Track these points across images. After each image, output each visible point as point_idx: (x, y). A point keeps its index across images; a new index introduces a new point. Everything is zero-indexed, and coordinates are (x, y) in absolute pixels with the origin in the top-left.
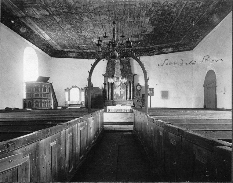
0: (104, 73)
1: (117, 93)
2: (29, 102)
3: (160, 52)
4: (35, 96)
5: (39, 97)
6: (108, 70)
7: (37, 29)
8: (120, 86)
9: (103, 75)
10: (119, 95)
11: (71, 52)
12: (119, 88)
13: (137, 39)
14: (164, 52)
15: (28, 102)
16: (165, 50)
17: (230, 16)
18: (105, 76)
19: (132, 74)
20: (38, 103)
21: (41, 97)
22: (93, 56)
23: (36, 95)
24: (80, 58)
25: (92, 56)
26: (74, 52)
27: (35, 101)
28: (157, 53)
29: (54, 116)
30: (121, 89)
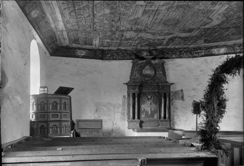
0: (127, 80)
1: (146, 110)
2: (42, 126)
3: (207, 53)
4: (52, 117)
5: (59, 119)
6: (133, 77)
7: (53, 13)
8: (150, 100)
9: (126, 84)
10: (150, 113)
11: (80, 49)
12: (149, 102)
13: (188, 35)
14: (213, 53)
15: (40, 126)
16: (215, 51)
17: (41, 1)
18: (129, 84)
19: (168, 82)
20: (57, 128)
21: (61, 118)
22: (110, 56)
23: (53, 116)
24: (62, 57)
25: (109, 55)
26: (84, 49)
27: (51, 124)
28: (203, 54)
29: (113, 151)
30: (152, 103)
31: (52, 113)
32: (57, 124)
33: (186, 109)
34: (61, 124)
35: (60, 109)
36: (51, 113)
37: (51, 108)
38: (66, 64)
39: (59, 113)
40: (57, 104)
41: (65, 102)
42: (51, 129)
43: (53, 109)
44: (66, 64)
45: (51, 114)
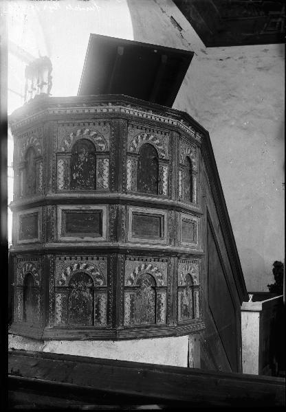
4: (69, 230)
20: (93, 290)
21: (116, 232)
31: (140, 210)
32: (96, 267)
33: (111, 236)
34: (114, 273)
35: (117, 178)
36: (61, 208)
37: (61, 177)
38: (260, 69)
39: (104, 208)
40: (94, 153)
41: (149, 149)
42: (59, 299)
43: (72, 184)
44: (260, 69)
45: (134, 213)
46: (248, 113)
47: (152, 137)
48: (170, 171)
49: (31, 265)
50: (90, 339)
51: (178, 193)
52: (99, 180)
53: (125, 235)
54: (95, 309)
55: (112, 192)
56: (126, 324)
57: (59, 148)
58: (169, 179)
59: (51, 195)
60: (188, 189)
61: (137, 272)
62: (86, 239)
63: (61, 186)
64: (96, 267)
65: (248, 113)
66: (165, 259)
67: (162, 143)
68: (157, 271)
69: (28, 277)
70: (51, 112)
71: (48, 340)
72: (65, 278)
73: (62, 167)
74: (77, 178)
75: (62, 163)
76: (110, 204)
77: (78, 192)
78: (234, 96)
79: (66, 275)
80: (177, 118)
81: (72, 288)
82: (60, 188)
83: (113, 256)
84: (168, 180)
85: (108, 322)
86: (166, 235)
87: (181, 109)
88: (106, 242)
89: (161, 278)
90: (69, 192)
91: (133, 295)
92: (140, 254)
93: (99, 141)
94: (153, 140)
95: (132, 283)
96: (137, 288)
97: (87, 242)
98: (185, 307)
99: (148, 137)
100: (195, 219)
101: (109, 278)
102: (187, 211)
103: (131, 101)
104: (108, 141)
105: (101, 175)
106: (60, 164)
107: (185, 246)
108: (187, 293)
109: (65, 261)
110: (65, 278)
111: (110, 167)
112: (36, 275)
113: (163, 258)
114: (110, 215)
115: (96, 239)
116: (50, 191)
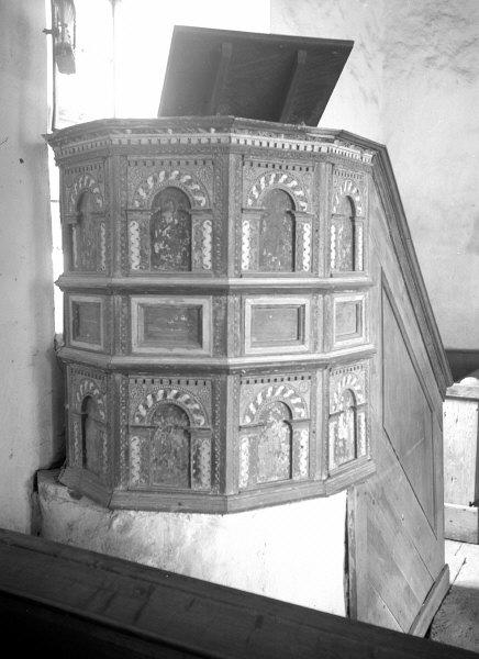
4: (150, 336)
31: (265, 300)
36: (135, 300)
37: (135, 249)
39: (207, 304)
46: (470, 44)
47: (285, 177)
48: (315, 231)
49: (92, 385)
50: (184, 511)
51: (329, 261)
52: (195, 256)
53: (240, 344)
54: (193, 462)
55: (218, 276)
56: (242, 485)
57: (130, 200)
58: (314, 243)
59: (120, 280)
60: (349, 250)
61: (260, 401)
62: (176, 351)
63: (135, 262)
64: (192, 396)
65: (470, 44)
66: (306, 375)
67: (298, 186)
68: (295, 395)
69: (87, 400)
70: (116, 142)
71: (118, 508)
72: (144, 412)
73: (137, 234)
74: (160, 251)
75: (136, 226)
76: (215, 295)
77: (162, 275)
78: (445, 15)
79: (146, 407)
80: (327, 140)
81: (154, 428)
82: (133, 267)
83: (215, 375)
84: (312, 245)
85: (213, 484)
86: (307, 337)
87: (338, 127)
88: (208, 356)
89: (301, 405)
90: (149, 275)
91: (254, 438)
92: (261, 371)
93: (195, 192)
94: (286, 181)
95: (252, 420)
96: (262, 425)
97: (179, 356)
98: (341, 444)
99: (277, 179)
100: (359, 297)
101: (214, 414)
102: (341, 288)
103: (247, 125)
104: (211, 192)
105: (200, 247)
106: (134, 229)
107: (342, 347)
108: (345, 420)
109: (144, 386)
110: (144, 412)
111: (214, 234)
112: (100, 402)
113: (303, 374)
114: (215, 312)
115: (191, 352)
116: (118, 273)
